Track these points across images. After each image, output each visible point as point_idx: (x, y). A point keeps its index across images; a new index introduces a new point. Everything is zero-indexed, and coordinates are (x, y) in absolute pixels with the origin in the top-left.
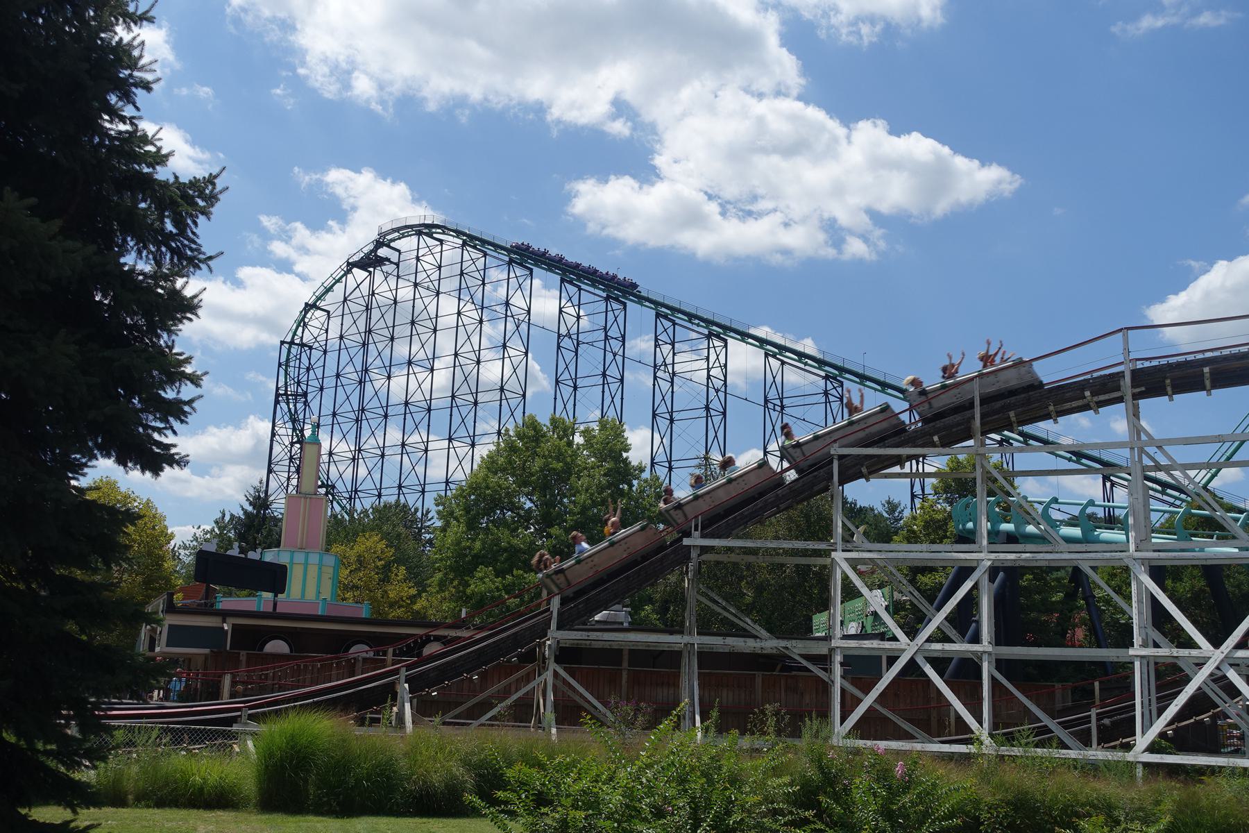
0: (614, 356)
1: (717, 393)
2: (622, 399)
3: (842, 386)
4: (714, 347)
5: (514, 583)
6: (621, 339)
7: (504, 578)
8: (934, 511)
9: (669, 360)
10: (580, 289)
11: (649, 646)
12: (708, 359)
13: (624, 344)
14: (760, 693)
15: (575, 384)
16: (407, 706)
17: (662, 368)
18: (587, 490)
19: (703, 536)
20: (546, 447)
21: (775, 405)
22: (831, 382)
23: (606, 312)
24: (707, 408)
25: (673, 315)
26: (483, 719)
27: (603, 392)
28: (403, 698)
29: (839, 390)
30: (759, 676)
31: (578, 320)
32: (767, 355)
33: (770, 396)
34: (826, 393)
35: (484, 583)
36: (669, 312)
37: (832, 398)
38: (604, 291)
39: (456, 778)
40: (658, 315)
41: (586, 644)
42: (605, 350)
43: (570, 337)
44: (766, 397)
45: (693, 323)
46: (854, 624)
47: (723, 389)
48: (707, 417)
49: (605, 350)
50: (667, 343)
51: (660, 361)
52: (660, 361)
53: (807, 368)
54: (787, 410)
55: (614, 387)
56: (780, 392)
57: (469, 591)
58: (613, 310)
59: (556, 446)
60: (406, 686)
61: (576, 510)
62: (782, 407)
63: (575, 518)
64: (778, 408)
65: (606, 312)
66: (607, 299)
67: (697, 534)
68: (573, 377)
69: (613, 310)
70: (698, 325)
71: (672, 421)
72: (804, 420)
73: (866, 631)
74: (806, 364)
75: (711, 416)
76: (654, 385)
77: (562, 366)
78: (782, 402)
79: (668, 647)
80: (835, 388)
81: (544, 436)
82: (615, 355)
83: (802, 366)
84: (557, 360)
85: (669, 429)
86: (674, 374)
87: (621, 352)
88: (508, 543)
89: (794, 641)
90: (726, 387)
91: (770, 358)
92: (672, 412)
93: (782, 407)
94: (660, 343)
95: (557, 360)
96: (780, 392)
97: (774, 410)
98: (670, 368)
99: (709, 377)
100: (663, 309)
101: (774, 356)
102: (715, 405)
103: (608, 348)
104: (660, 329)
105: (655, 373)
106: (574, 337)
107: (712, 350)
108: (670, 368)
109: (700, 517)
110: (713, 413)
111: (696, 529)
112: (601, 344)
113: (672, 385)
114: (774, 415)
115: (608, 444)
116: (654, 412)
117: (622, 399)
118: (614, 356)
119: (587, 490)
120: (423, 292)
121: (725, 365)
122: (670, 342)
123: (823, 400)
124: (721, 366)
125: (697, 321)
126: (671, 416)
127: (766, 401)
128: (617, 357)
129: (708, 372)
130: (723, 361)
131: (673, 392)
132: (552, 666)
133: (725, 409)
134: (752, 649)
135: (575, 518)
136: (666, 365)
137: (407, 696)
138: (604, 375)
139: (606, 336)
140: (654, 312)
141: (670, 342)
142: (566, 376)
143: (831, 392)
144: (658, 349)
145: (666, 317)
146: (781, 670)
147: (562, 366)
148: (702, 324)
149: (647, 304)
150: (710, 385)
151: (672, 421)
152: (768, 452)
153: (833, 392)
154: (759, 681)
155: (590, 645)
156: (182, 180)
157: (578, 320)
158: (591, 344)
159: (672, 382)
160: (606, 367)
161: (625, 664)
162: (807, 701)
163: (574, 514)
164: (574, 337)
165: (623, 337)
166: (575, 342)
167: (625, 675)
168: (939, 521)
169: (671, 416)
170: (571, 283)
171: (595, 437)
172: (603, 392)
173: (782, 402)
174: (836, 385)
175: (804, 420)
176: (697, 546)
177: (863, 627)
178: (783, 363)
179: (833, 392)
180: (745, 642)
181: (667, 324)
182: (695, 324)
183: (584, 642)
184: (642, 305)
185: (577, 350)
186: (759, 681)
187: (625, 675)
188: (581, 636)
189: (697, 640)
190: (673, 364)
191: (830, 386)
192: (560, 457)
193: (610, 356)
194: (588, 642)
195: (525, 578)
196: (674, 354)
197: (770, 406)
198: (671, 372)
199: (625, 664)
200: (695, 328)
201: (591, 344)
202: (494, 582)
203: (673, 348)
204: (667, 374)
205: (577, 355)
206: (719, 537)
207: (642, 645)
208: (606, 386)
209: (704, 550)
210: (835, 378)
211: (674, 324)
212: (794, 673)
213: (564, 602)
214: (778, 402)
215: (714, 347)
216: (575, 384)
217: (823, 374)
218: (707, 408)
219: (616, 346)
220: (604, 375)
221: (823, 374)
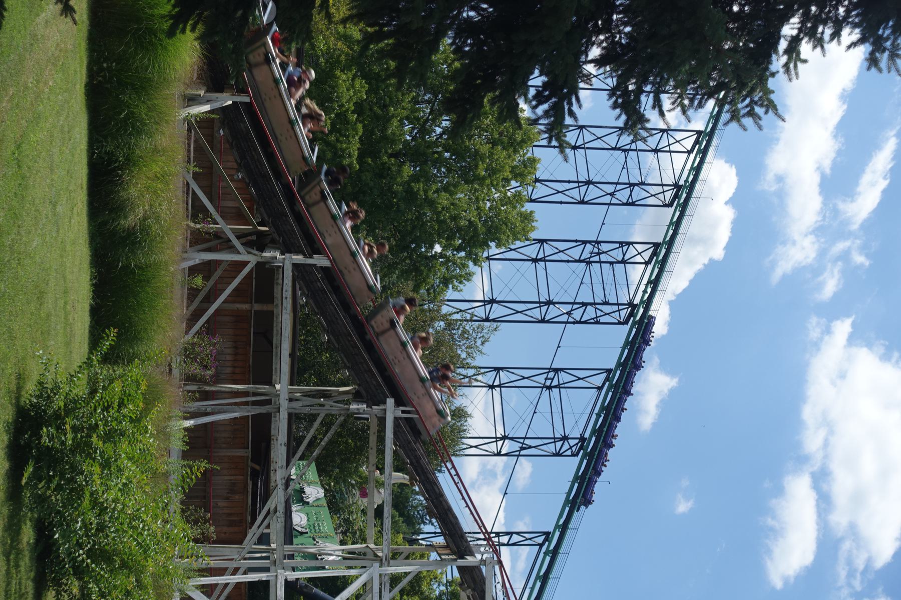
0: (610, 194)
1: (567, 313)
2: (561, 203)
3: (573, 455)
4: (619, 310)
5: (348, 123)
6: (630, 201)
7: (353, 112)
8: (431, 580)
9: (604, 257)
10: (689, 152)
11: (277, 347)
12: (606, 303)
13: (624, 204)
14: (229, 454)
15: (579, 147)
16: (207, 108)
17: (596, 250)
18: (453, 204)
19: (396, 419)
20: (501, 153)
21: (552, 379)
22: (577, 444)
23: (662, 185)
24: (549, 303)
25: (656, 262)
26: (194, 186)
27: (569, 182)
28: (216, 100)
29: (569, 453)
30: (247, 453)
31: (652, 150)
32: (609, 371)
33: (562, 375)
34: (565, 438)
35: (348, 90)
36: (661, 258)
37: (559, 444)
38: (686, 181)
39: (132, 209)
40: (656, 246)
41: (278, 279)
42: (617, 183)
43: (633, 141)
44: (562, 370)
45: (647, 285)
46: (304, 521)
47: (571, 320)
48: (539, 302)
49: (617, 183)
50: (624, 255)
51: (604, 247)
52: (604, 247)
53: (594, 417)
54: (546, 393)
55: (575, 193)
56: (566, 385)
57: (338, 73)
58: (664, 192)
59: (503, 167)
60: (230, 102)
61: (430, 193)
62: (550, 388)
63: (421, 193)
64: (548, 383)
65: (662, 185)
66: (676, 186)
67: (399, 414)
68: (587, 145)
69: (664, 192)
70: (645, 292)
71: (535, 261)
72: (535, 412)
73: (296, 537)
74: (598, 415)
75: (540, 307)
76: (576, 241)
77: (600, 132)
78: (555, 387)
79: (276, 368)
80: (571, 448)
81: (516, 151)
82: (612, 194)
83: (596, 411)
84: (606, 127)
85: (526, 258)
86: (589, 263)
87: (614, 201)
88: (393, 116)
89: (283, 519)
90: (574, 323)
91: (605, 375)
92: (545, 261)
93: (550, 388)
94: (625, 248)
95: (606, 127)
96: (566, 385)
97: (546, 379)
98: (596, 259)
99: (585, 304)
100: (663, 251)
101: (607, 379)
102: (553, 312)
103: (619, 187)
104: (640, 248)
105: (590, 242)
106: (633, 146)
107: (615, 308)
108: (596, 259)
109: (417, 416)
110: (544, 309)
111: (403, 412)
112: (624, 179)
113: (576, 261)
114: (541, 379)
115: (506, 224)
116: (546, 241)
117: (561, 203)
118: (610, 194)
119: (453, 204)
120: (664, 143)
121: (598, 323)
122: (626, 259)
123: (558, 435)
124: (597, 317)
125: (649, 290)
126: (541, 260)
127: (556, 370)
128: (609, 197)
129: (590, 304)
130: (602, 320)
131: (568, 261)
132: (251, 259)
133: (548, 322)
134: (275, 460)
135: (421, 193)
136: (599, 254)
137: (217, 105)
138: (589, 183)
139: (633, 185)
140: (660, 240)
141: (626, 259)
142: (588, 137)
143: (566, 443)
144: (617, 245)
145: (655, 254)
146: (253, 469)
147: (600, 132)
148: (647, 296)
149: (671, 232)
150: (575, 306)
151: (535, 261)
152: (498, 372)
153: (566, 446)
154: (240, 453)
155: (277, 284)
156: (770, 80)
157: (652, 150)
158: (625, 166)
159: (579, 261)
160: (598, 185)
161: (257, 307)
162: (219, 504)
163: (426, 192)
164: (633, 146)
165: (633, 204)
166: (627, 147)
167: (246, 306)
168: (420, 587)
169: (541, 260)
170: (697, 142)
171: (515, 207)
172: (569, 182)
173: (555, 387)
174: (574, 449)
175: (535, 412)
176: (385, 413)
177: (302, 533)
178: (600, 389)
179: (566, 446)
180: (282, 467)
181: (647, 256)
182: (646, 288)
183: (281, 276)
184: (669, 226)
185: (619, 149)
186: (240, 453)
187: (246, 306)
188: (286, 291)
189: (282, 386)
190: (600, 262)
191: (572, 442)
192: (492, 172)
193: (610, 189)
194: (280, 281)
195: (354, 137)
196: (611, 263)
197: (551, 375)
198: (592, 259)
199: (257, 307)
200: (642, 287)
201: (625, 166)
202: (349, 101)
203: (619, 262)
204: (589, 256)
205: (613, 149)
206: (395, 433)
207: (277, 339)
208: (576, 185)
209: (382, 420)
210: (581, 448)
211: (647, 263)
212: (250, 483)
213: (324, 269)
214: (555, 383)
215: (619, 310)
216: (579, 147)
217: (587, 435)
218: (549, 303)
219: (623, 196)
220: (589, 183)
221: (587, 435)
